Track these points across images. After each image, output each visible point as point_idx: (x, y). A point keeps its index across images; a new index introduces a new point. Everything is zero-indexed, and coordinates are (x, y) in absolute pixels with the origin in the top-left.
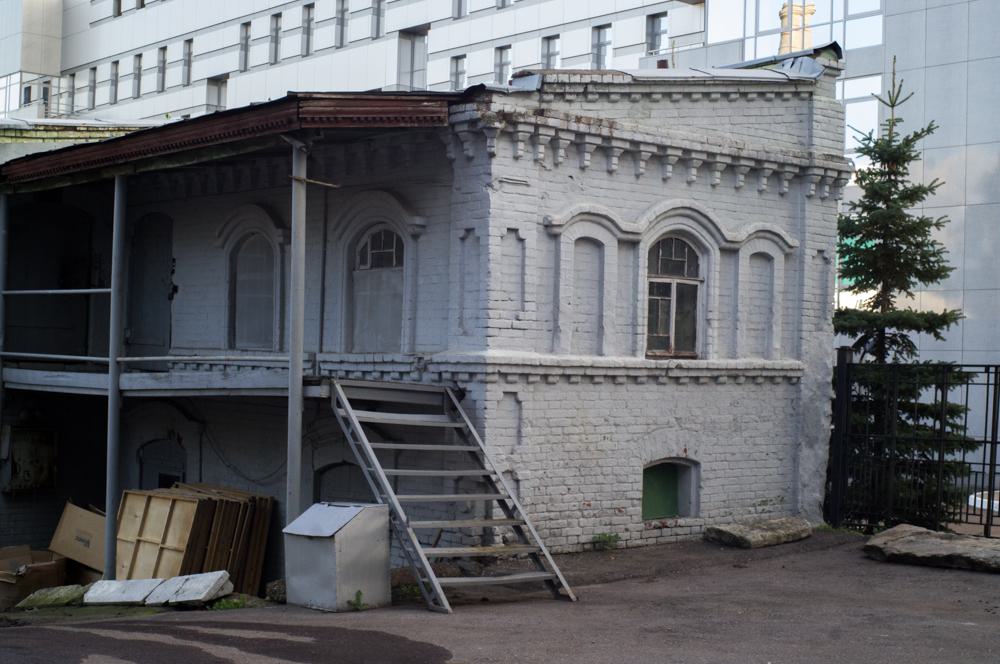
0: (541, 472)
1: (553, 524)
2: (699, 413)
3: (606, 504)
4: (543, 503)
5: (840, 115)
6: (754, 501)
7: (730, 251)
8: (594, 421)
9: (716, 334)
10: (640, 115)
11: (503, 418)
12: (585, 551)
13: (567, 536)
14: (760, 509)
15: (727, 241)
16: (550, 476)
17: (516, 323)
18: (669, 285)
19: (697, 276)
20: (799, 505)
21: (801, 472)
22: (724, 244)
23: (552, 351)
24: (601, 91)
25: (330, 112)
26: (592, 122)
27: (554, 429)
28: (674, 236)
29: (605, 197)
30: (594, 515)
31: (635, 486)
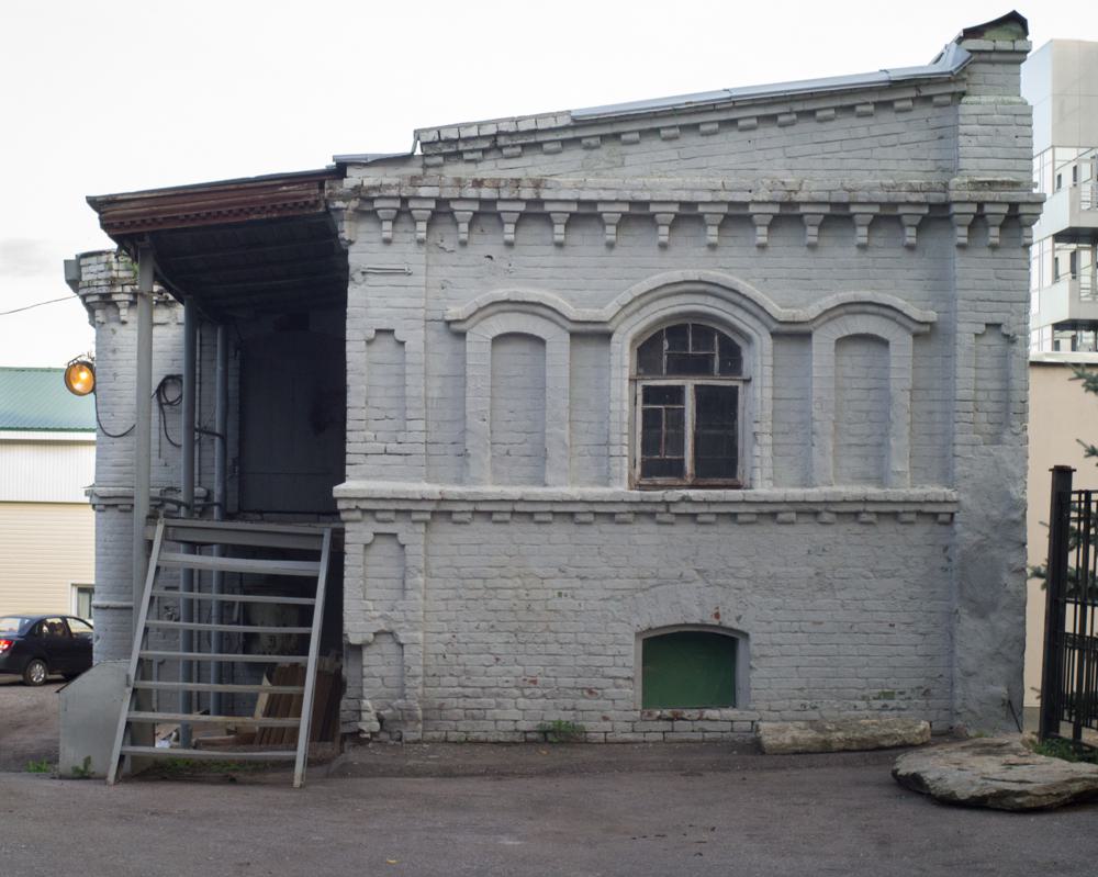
0: (448, 636)
1: (470, 703)
2: (742, 564)
3: (570, 682)
4: (452, 675)
5: (1025, 120)
6: (866, 693)
7: (794, 335)
8: (540, 572)
9: (767, 452)
10: (602, 165)
11: (380, 565)
12: (528, 742)
13: (496, 721)
14: (878, 704)
15: (776, 320)
16: (462, 640)
17: (392, 447)
18: (680, 390)
19: (740, 374)
20: (958, 702)
21: (959, 652)
22: (775, 327)
23: (459, 481)
24: (523, 141)
25: (145, 214)
26: (502, 184)
27: (468, 582)
28: (690, 322)
29: (552, 277)
30: (544, 696)
31: (632, 654)
